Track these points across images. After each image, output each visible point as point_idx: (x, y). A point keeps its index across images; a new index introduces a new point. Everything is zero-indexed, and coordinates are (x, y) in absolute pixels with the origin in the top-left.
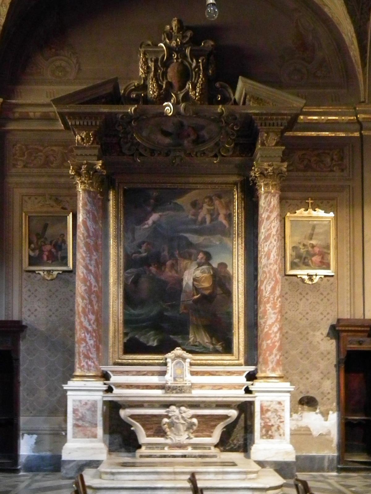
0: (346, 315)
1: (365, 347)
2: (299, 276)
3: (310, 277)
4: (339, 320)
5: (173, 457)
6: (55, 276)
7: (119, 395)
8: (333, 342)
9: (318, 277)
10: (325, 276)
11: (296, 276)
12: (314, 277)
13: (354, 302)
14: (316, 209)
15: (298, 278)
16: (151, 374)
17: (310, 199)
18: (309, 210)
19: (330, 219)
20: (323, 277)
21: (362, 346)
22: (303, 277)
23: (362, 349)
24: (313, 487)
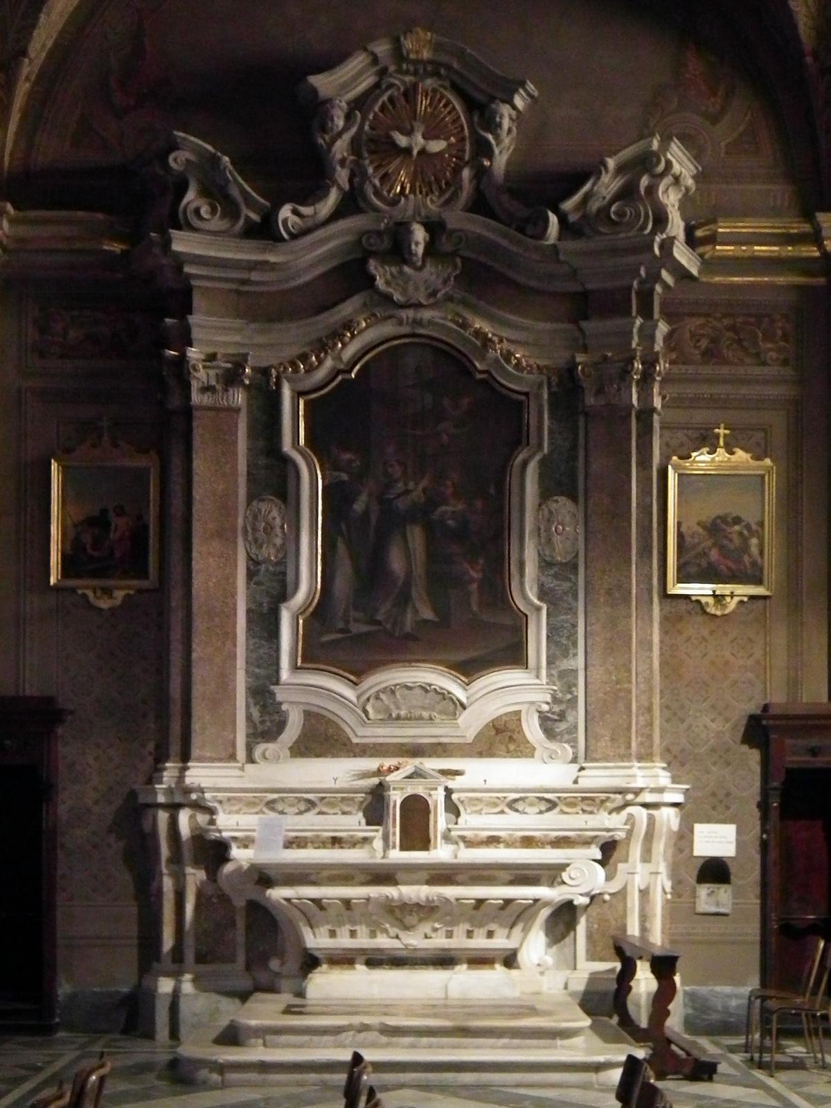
0: (778, 698)
1: (821, 761)
2: (694, 598)
3: (718, 598)
4: (766, 708)
5: (183, 734)
6: (118, 602)
7: (349, 1009)
8: (754, 757)
9: (736, 599)
10: (752, 598)
11: (687, 597)
12: (728, 599)
13: (442, 1047)
14: (735, 450)
15: (691, 601)
16: (348, 846)
17: (722, 425)
18: (718, 450)
19: (763, 472)
20: (745, 599)
21: (817, 759)
22: (703, 600)
23: (819, 765)
24: (376, 1086)
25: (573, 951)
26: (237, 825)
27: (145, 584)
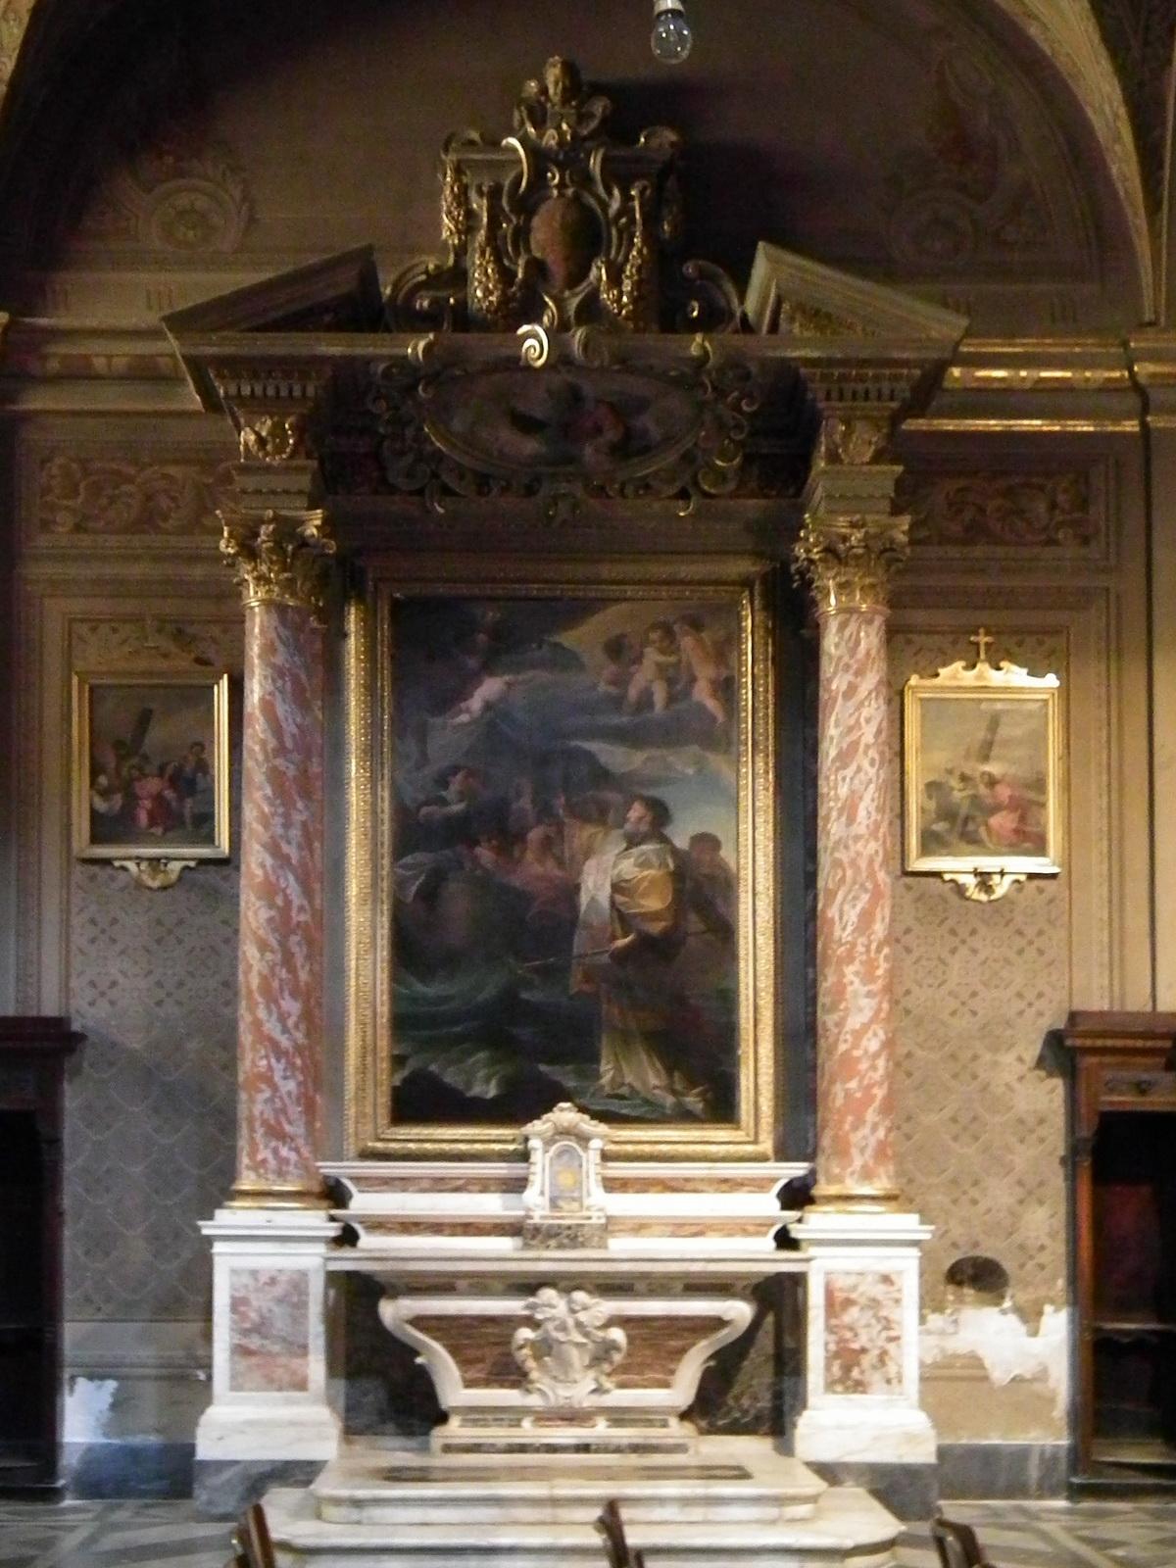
1: (1158, 1101)
2: (947, 877)
3: (984, 879)
4: (1073, 1016)
5: (547, 1452)
6: (174, 877)
8: (1057, 1086)
9: (1008, 879)
10: (1031, 876)
11: (938, 875)
12: (996, 878)
13: (1122, 960)
14: (1003, 664)
15: (944, 881)
16: (477, 1188)
17: (982, 631)
18: (979, 666)
19: (1045, 697)
21: (1148, 1099)
22: (962, 879)
23: (1149, 1108)
25: (408, 1528)
26: (93, 878)
27: (204, 852)
